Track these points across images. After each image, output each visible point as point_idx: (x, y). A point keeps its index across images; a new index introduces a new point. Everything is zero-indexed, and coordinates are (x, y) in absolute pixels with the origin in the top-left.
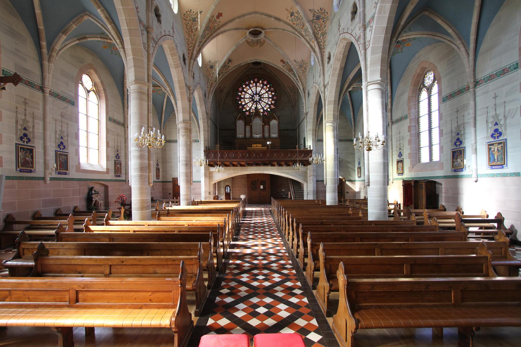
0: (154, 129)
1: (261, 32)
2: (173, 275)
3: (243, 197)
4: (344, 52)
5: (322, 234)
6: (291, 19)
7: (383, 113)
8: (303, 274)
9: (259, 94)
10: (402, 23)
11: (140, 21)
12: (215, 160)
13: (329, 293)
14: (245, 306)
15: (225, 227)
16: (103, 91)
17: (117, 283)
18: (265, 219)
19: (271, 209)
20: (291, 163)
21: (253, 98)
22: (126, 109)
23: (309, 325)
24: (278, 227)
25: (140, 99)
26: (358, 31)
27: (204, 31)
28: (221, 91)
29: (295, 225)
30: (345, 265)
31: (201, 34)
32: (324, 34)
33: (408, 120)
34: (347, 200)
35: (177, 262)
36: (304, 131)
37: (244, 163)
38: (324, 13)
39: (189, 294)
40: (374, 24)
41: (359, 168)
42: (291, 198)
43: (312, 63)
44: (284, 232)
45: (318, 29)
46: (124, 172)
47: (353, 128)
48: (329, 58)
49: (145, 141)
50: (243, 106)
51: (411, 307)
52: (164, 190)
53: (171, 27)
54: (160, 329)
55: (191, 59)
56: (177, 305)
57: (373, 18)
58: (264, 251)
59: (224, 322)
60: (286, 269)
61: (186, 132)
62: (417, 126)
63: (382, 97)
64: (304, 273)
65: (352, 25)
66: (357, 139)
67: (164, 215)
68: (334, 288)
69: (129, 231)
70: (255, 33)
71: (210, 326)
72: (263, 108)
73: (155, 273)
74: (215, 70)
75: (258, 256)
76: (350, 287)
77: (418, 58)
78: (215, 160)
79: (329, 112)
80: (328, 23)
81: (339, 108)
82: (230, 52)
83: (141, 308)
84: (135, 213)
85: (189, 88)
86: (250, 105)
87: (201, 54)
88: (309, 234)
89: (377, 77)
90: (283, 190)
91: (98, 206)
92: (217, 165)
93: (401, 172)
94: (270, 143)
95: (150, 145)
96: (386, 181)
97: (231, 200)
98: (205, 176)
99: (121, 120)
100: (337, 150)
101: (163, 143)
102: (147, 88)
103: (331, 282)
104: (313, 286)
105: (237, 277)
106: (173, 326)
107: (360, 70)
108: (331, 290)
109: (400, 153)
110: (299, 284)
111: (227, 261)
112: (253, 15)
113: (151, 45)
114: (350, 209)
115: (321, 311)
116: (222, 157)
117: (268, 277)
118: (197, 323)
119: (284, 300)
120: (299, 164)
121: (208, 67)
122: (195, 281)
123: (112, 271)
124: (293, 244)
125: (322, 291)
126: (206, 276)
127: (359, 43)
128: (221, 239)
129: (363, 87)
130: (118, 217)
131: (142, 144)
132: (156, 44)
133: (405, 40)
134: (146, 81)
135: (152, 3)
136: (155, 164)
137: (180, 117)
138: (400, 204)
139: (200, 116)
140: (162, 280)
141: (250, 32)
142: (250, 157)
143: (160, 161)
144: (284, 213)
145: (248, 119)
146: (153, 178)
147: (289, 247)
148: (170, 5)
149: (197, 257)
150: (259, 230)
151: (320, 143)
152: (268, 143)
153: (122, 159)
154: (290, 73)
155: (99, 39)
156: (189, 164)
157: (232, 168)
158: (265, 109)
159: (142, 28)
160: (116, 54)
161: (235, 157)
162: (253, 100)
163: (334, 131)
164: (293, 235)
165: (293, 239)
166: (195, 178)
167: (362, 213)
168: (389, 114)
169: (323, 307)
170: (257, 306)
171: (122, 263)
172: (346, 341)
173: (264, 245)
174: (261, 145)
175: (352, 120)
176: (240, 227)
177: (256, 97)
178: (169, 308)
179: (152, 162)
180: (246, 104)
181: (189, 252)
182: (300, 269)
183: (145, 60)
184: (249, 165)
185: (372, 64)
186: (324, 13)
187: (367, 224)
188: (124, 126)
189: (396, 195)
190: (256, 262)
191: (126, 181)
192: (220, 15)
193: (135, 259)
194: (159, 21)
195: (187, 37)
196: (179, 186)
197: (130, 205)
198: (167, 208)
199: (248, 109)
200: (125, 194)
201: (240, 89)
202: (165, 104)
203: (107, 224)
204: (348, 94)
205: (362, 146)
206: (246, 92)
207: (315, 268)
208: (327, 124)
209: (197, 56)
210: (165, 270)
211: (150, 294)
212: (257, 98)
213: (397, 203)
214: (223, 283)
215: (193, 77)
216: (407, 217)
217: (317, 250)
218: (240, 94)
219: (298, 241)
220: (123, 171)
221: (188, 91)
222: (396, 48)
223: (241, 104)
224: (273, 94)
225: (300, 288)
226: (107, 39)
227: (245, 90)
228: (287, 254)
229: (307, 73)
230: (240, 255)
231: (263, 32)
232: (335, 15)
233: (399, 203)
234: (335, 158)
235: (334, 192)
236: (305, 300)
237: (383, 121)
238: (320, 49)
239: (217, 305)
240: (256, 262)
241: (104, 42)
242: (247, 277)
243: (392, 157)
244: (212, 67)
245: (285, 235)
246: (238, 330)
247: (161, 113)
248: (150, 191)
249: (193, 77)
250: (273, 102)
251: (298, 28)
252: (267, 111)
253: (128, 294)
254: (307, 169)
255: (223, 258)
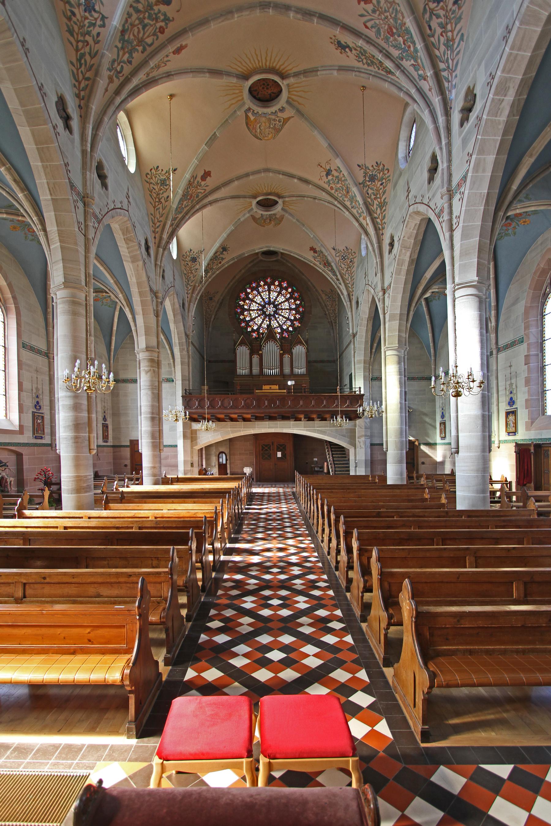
0: (96, 362)
1: (276, 203)
2: (126, 599)
3: (248, 470)
4: (417, 234)
5: (379, 533)
6: (326, 180)
7: (481, 335)
8: (346, 597)
9: (273, 303)
10: (514, 187)
11: (72, 186)
12: (200, 411)
13: (388, 628)
14: (249, 649)
15: (216, 520)
16: (11, 301)
17: (34, 613)
18: (284, 507)
19: (294, 490)
20: (327, 416)
21: (265, 310)
22: (51, 329)
23: (354, 679)
24: (305, 519)
25: (74, 314)
26: (440, 202)
27: (181, 200)
28: (211, 299)
29: (333, 517)
30: (412, 583)
31: (174, 206)
32: (382, 205)
33: (524, 346)
34: (421, 476)
35: (134, 579)
36: (349, 363)
37: (249, 416)
38: (383, 170)
39: (154, 630)
40: (466, 189)
41: (443, 424)
42: (328, 472)
43: (364, 253)
44: (315, 528)
45: (373, 197)
46: (49, 431)
47: (433, 358)
48: (392, 245)
49: (81, 382)
50: (247, 323)
51: (524, 652)
52: (116, 459)
53: (125, 194)
54: (105, 686)
55: (158, 247)
56: (133, 648)
57: (464, 178)
58: (281, 559)
59: (212, 674)
60: (318, 588)
61: (152, 366)
62: (540, 355)
63: (480, 309)
64: (348, 594)
65: (429, 190)
66: (437, 377)
67: (115, 501)
68: (395, 621)
69: (57, 527)
70: (267, 204)
71: (190, 681)
72: (280, 326)
73: (99, 596)
74: (200, 265)
75: (271, 567)
76: (421, 620)
77: (542, 243)
78: (200, 411)
79: (391, 332)
80: (389, 186)
81: (409, 325)
82: (225, 235)
83: (74, 652)
84: (67, 497)
85: (155, 294)
86: (259, 321)
87: (175, 240)
88: (355, 532)
89: (473, 276)
90: (316, 459)
91: (6, 486)
92: (204, 418)
93: (513, 430)
94: (293, 382)
95: (89, 388)
96: (487, 446)
97: (229, 476)
98: (185, 437)
99: (43, 347)
100: (404, 395)
101: (112, 384)
102: (84, 295)
103: (391, 611)
104: (361, 616)
105: (235, 602)
106: (127, 682)
107: (443, 263)
108: (390, 624)
109: (511, 399)
110: (338, 613)
111: (219, 576)
112: (263, 174)
113: (91, 224)
114: (427, 490)
115: (376, 658)
116: (212, 406)
117: (287, 602)
118: (168, 676)
119: (303, 639)
120: (342, 417)
121: (188, 259)
122: (164, 609)
123: (27, 593)
124: (329, 548)
125: (376, 625)
126: (183, 599)
127: (441, 220)
128: (208, 540)
129: (448, 292)
130: (39, 504)
131: (76, 386)
132: (99, 223)
133: (520, 214)
134: (83, 283)
135: (92, 156)
136: (100, 418)
137: (141, 342)
138: (510, 483)
139: (175, 340)
140: (109, 607)
141: (258, 203)
142: (259, 406)
143: (109, 412)
144: (315, 497)
145: (255, 346)
146: (97, 439)
147: (323, 553)
148: (121, 159)
149: (167, 570)
150: (274, 526)
151: (376, 383)
152: (289, 383)
153: (46, 410)
154: (326, 269)
155: (5, 216)
156: (156, 418)
157: (230, 423)
158: (285, 327)
159: (75, 198)
160: (33, 240)
161: (235, 407)
162: (264, 313)
163: (399, 363)
164: (330, 533)
165: (330, 540)
166: (167, 441)
167: (446, 498)
168: (493, 336)
169: (379, 652)
170: (268, 648)
171: (43, 581)
172: (415, 706)
173: (281, 550)
174: (277, 387)
175: (431, 345)
176: (243, 519)
177: (269, 308)
178: (120, 653)
179: (94, 416)
180: (252, 320)
181: (155, 562)
182: (341, 590)
183: (82, 250)
184: (258, 418)
185: (464, 253)
186: (383, 170)
187: (453, 516)
188: (48, 357)
189: (504, 466)
190: (267, 577)
191: (52, 446)
192: (207, 174)
193: (65, 574)
194: (104, 185)
195: (152, 210)
196: (141, 454)
197: (59, 484)
198: (121, 489)
199: (255, 328)
200: (51, 467)
201: (243, 295)
202: (116, 320)
203: (21, 516)
204: (423, 303)
205: (445, 389)
206: (252, 301)
207: (365, 587)
208: (388, 353)
209: (169, 241)
210: (115, 591)
211: (88, 630)
212: (270, 309)
213: (506, 481)
214: (213, 612)
215: (163, 277)
216: (521, 504)
217: (369, 558)
218: (241, 303)
219: (338, 544)
220: (47, 430)
221: (154, 299)
222: (505, 228)
223: (244, 320)
224: (298, 302)
225: (340, 620)
226: (18, 215)
227: (250, 296)
228: (320, 564)
229: (354, 269)
230: (241, 565)
231: (280, 201)
232: (400, 174)
233: (509, 480)
234: (401, 408)
235: (400, 462)
236: (349, 639)
237: (482, 348)
238: (376, 229)
239: (201, 647)
240: (267, 577)
241: (12, 221)
242: (253, 602)
243: (498, 405)
244: (194, 260)
245: (317, 532)
246: (236, 687)
247: (108, 336)
248: (91, 462)
249: (163, 277)
250: (298, 316)
251: (338, 195)
252: (287, 330)
253: (52, 631)
254: (355, 426)
255: (214, 571)
